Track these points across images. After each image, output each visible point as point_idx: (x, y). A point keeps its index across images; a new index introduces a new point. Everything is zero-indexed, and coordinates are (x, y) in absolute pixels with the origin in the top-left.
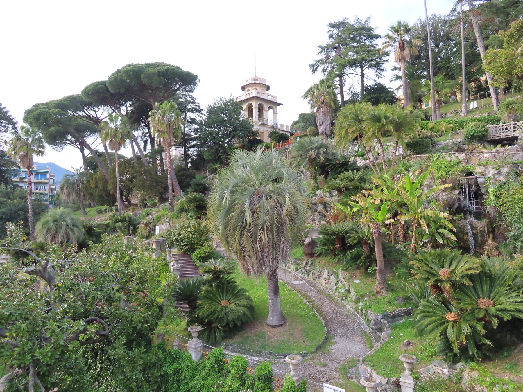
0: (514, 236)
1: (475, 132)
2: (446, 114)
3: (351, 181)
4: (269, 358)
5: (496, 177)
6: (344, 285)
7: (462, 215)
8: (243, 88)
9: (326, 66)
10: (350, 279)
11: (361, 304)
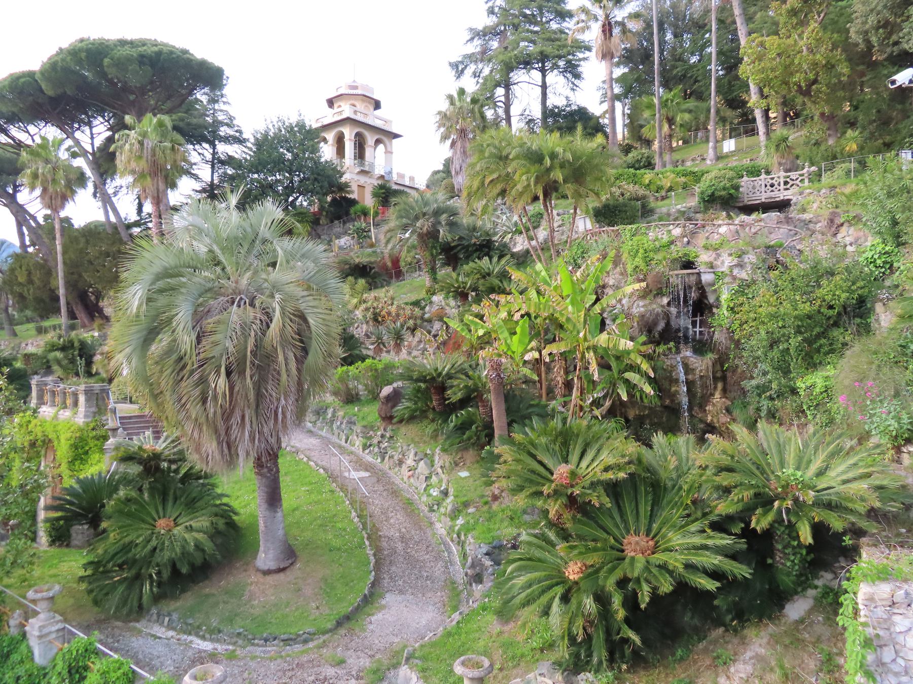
0: (758, 387)
1: (716, 189)
2: (683, 161)
3: (484, 277)
4: (234, 644)
5: (736, 271)
6: (441, 480)
7: (672, 344)
8: (331, 103)
9: (480, 66)
10: (453, 469)
11: (460, 521)
